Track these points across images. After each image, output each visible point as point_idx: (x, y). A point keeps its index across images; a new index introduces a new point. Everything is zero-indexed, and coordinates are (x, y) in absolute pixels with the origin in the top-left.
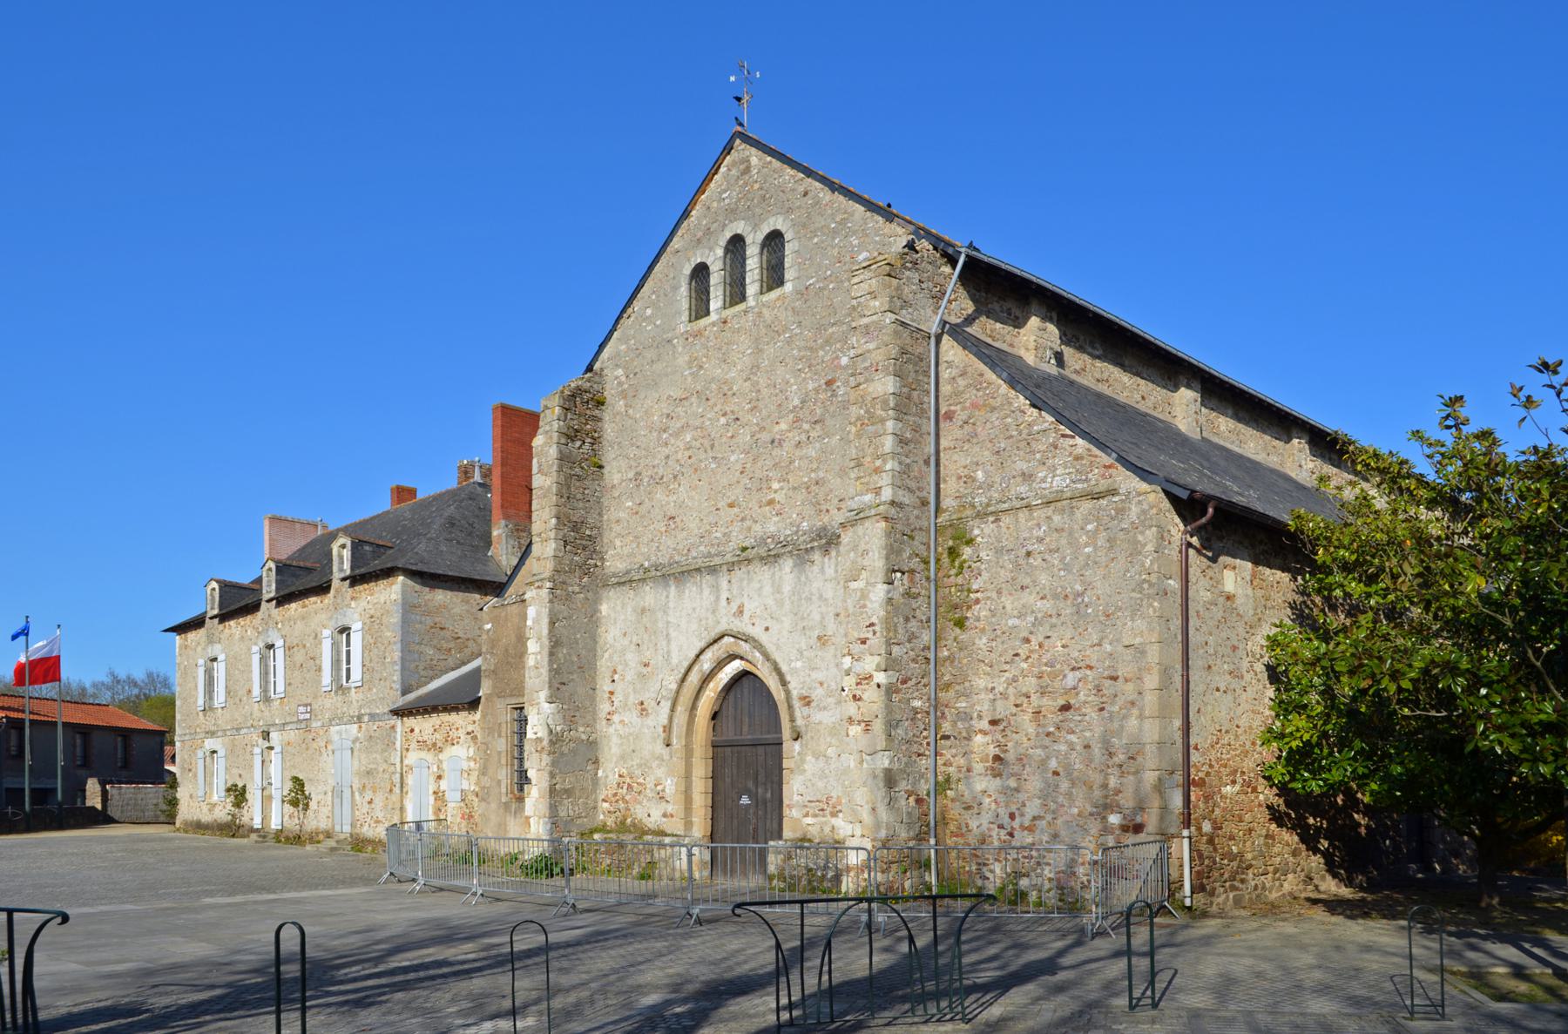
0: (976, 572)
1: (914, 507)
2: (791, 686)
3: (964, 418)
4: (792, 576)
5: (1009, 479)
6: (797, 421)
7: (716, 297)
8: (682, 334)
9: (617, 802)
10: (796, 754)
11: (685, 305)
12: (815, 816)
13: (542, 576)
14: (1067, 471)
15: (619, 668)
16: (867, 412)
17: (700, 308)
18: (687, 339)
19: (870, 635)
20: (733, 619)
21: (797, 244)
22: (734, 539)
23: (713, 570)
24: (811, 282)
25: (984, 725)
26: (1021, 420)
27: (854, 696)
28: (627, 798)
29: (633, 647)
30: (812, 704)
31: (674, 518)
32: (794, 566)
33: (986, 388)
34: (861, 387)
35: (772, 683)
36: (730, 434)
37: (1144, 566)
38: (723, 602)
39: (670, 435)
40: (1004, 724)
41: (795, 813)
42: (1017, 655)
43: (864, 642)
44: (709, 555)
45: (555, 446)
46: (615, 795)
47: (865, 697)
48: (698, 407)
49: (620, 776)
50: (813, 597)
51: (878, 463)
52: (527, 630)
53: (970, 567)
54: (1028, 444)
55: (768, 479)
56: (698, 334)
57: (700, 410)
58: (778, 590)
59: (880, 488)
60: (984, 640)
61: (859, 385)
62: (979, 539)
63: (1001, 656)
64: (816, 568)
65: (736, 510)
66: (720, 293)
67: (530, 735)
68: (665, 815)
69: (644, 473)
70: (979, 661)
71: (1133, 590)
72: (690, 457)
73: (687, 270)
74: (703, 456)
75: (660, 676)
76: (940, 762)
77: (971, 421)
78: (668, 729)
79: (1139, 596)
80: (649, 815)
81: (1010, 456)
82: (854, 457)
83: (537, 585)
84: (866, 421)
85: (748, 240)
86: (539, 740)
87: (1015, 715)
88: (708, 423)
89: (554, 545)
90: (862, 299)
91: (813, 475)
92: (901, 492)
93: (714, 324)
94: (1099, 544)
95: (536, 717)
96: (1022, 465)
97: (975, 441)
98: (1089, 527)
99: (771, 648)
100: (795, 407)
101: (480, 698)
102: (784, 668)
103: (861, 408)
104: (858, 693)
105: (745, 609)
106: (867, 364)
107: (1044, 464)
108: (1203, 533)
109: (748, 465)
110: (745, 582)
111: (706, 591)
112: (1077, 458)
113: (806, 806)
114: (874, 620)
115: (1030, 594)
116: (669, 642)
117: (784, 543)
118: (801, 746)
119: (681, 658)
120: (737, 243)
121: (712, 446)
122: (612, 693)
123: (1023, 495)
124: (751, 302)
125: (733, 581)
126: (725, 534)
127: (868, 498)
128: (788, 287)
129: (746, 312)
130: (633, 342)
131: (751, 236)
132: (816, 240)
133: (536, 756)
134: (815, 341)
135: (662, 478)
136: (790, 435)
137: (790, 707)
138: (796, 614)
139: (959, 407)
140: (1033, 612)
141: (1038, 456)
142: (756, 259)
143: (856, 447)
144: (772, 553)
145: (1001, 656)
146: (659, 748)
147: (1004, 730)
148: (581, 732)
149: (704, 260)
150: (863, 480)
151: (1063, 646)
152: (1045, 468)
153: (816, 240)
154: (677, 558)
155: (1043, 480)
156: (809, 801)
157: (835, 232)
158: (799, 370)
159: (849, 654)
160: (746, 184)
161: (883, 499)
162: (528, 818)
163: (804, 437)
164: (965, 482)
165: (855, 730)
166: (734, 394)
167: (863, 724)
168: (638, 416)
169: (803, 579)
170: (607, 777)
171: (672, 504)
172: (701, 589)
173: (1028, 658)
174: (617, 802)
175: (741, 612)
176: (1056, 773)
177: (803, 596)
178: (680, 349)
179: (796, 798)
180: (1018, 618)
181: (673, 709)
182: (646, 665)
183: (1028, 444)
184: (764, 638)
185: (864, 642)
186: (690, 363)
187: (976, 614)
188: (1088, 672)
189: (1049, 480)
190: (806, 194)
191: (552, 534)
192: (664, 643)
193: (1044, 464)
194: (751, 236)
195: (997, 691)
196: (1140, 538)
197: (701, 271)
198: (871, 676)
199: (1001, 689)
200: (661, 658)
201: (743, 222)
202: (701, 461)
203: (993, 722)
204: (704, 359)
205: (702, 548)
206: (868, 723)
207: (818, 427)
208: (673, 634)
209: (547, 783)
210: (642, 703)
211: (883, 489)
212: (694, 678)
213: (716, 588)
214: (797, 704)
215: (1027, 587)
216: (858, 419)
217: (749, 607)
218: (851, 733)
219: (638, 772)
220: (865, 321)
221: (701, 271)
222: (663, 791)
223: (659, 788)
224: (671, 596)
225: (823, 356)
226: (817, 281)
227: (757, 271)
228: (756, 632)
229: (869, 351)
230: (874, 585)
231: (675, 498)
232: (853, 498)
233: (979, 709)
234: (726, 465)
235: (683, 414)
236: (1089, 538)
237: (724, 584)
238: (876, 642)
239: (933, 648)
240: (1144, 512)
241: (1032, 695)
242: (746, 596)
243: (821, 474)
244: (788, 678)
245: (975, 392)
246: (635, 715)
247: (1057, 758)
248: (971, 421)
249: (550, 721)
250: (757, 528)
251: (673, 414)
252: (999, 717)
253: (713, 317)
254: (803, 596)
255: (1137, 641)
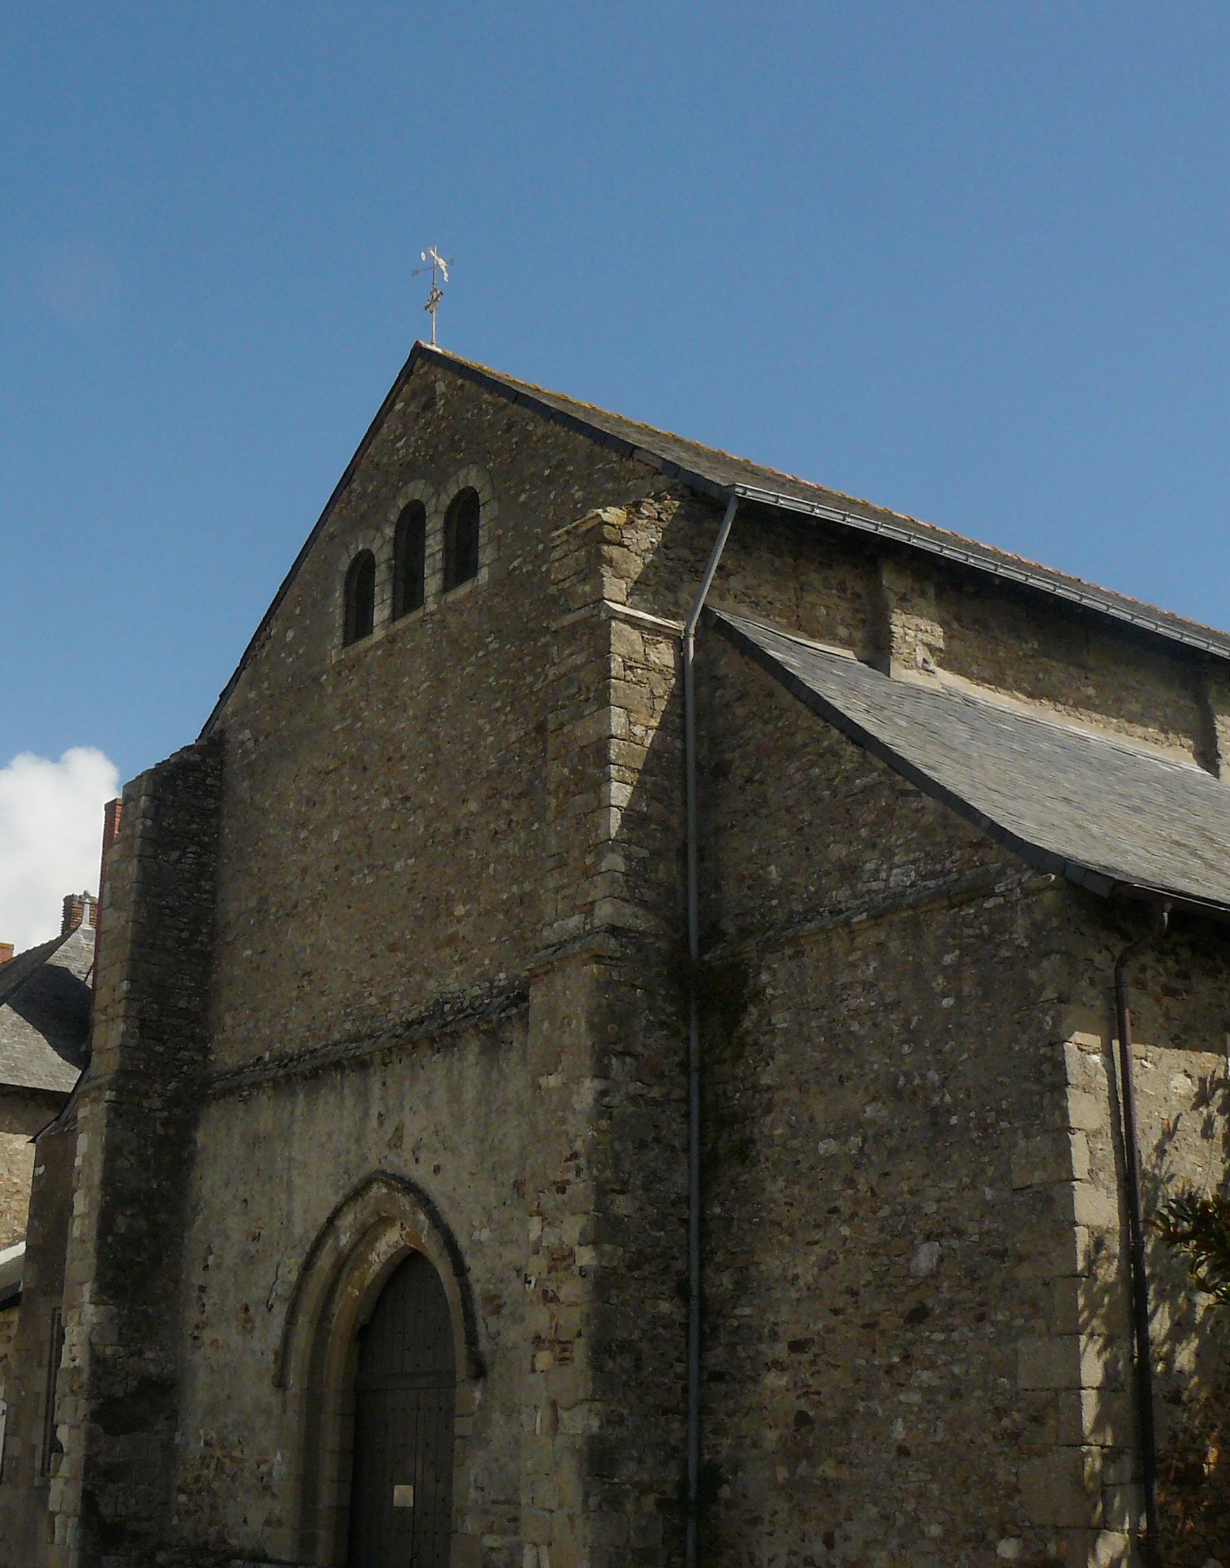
0: (766, 1051)
1: (656, 936)
2: (472, 1276)
3: (746, 772)
4: (478, 1070)
5: (819, 878)
6: (493, 796)
7: (383, 601)
8: (334, 667)
9: (199, 1492)
10: (475, 1408)
11: (339, 620)
12: (504, 1532)
13: (99, 1081)
14: (912, 857)
15: (216, 1243)
16: (573, 770)
17: (358, 625)
18: (339, 673)
19: (571, 1176)
20: (386, 1152)
21: (496, 506)
22: (395, 1007)
23: (362, 1065)
24: (516, 564)
25: (780, 1350)
26: (834, 770)
27: (545, 1292)
28: (215, 1485)
29: (238, 1205)
30: (505, 1311)
31: (309, 974)
32: (481, 1053)
33: (780, 717)
34: (565, 729)
35: (444, 1269)
36: (394, 826)
37: (1041, 1029)
38: (374, 1122)
39: (310, 832)
40: (815, 1349)
41: (471, 1525)
42: (835, 1210)
43: (562, 1190)
44: (357, 1038)
45: (135, 861)
46: (197, 1479)
47: (561, 1295)
48: (351, 783)
49: (207, 1444)
50: (510, 1109)
51: (589, 860)
52: (75, 1175)
53: (756, 1043)
54: (848, 811)
55: (450, 899)
56: (355, 664)
57: (354, 788)
58: (455, 1096)
59: (592, 903)
60: (781, 1183)
61: (562, 725)
62: (769, 991)
63: (807, 1212)
64: (514, 1056)
65: (400, 956)
66: (387, 595)
67: (65, 1363)
68: (268, 1522)
69: (272, 899)
70: (772, 1223)
71: (1026, 1078)
72: (336, 868)
73: (344, 565)
74: (356, 865)
75: (276, 1258)
76: (708, 1427)
77: (757, 777)
78: (282, 1356)
79: (1036, 1088)
80: (245, 1521)
81: (820, 836)
82: (554, 850)
83: (93, 1095)
84: (572, 788)
85: (429, 510)
86: (77, 1370)
87: (833, 1330)
88: (364, 809)
89: (122, 1027)
90: (567, 584)
91: (515, 889)
92: (628, 910)
93: (377, 646)
94: (966, 990)
95: (76, 1330)
96: (838, 851)
97: (764, 811)
98: (948, 959)
99: (442, 1204)
100: (490, 773)
101: (21, 1293)
102: (462, 1242)
103: (564, 766)
104: (551, 1286)
105: (406, 1131)
106: (574, 690)
107: (874, 846)
108: (1170, 963)
109: (420, 877)
110: (407, 1083)
111: (349, 1102)
112: (927, 832)
113: (486, 1512)
114: (578, 1145)
115: (855, 1090)
116: (290, 1198)
117: (470, 1011)
118: (484, 1392)
119: (304, 1227)
120: (414, 517)
121: (369, 846)
122: (202, 1289)
123: (842, 906)
124: (431, 606)
125: (389, 1083)
126: (383, 997)
127: (574, 921)
128: (484, 575)
129: (423, 621)
130: (266, 685)
131: (434, 501)
132: (523, 497)
133: (70, 1400)
134: (520, 659)
135: (295, 906)
136: (483, 820)
137: (469, 1317)
138: (482, 1141)
139: (737, 754)
140: (860, 1125)
141: (864, 832)
142: (439, 537)
143: (557, 834)
144: (448, 1029)
145: (807, 1212)
146: (265, 1392)
147: (813, 1362)
148: (151, 1360)
149: (368, 547)
150: (566, 892)
151: (911, 1192)
152: (877, 854)
153: (523, 497)
154: (311, 1045)
155: (875, 875)
156: (495, 1502)
157: (550, 480)
158: (497, 710)
159: (539, 1213)
160: (428, 424)
161: (597, 922)
162: (53, 1515)
163: (502, 824)
164: (749, 888)
165: (544, 1359)
166: (403, 758)
167: (558, 1348)
168: (267, 804)
169: (495, 1075)
170: (187, 1444)
171: (308, 950)
172: (343, 1098)
173: (854, 1215)
174: (199, 1492)
175: (400, 1138)
176: (903, 1451)
177: (494, 1108)
178: (330, 690)
179: (473, 1494)
180: (835, 1137)
181: (291, 1319)
182: (256, 1238)
183: (848, 811)
184: (433, 1187)
185: (562, 1190)
186: (342, 711)
187: (766, 1132)
188: (955, 1243)
189: (883, 875)
190: (509, 428)
191: (121, 1009)
192: (283, 1196)
193: (874, 846)
194: (434, 501)
195: (801, 1282)
196: (1033, 975)
197: (364, 566)
198: (571, 1254)
199: (810, 1279)
200: (278, 1225)
201: (423, 481)
202: (352, 873)
203: (797, 1346)
204: (362, 704)
205: (348, 1026)
206: (565, 1345)
207: (524, 804)
208: (298, 1181)
209: (82, 1452)
210: (247, 1309)
211: (597, 904)
212: (325, 1262)
213: (363, 1095)
214: (480, 1310)
215: (849, 1078)
216: (559, 784)
217: (415, 1127)
218: (539, 1366)
219: (234, 1438)
220: (569, 619)
221: (364, 566)
222: (270, 1473)
223: (264, 1468)
224: (298, 1112)
225: (531, 685)
226: (525, 562)
227: (439, 556)
228: (420, 1173)
229: (577, 669)
230: (578, 1081)
231: (313, 938)
232: (551, 924)
233: (772, 1318)
234: (388, 877)
235: (329, 797)
236: (947, 978)
237: (376, 1090)
238: (580, 1188)
239: (694, 1199)
240: (1036, 926)
241: (862, 1291)
242: (407, 1109)
243: (527, 887)
244: (468, 1261)
245: (761, 725)
246: (234, 1331)
247: (904, 1418)
248: (757, 777)
249: (95, 1339)
250: (431, 984)
251: (316, 798)
252: (808, 1335)
253: (378, 634)
254: (494, 1108)
255: (1037, 1178)
